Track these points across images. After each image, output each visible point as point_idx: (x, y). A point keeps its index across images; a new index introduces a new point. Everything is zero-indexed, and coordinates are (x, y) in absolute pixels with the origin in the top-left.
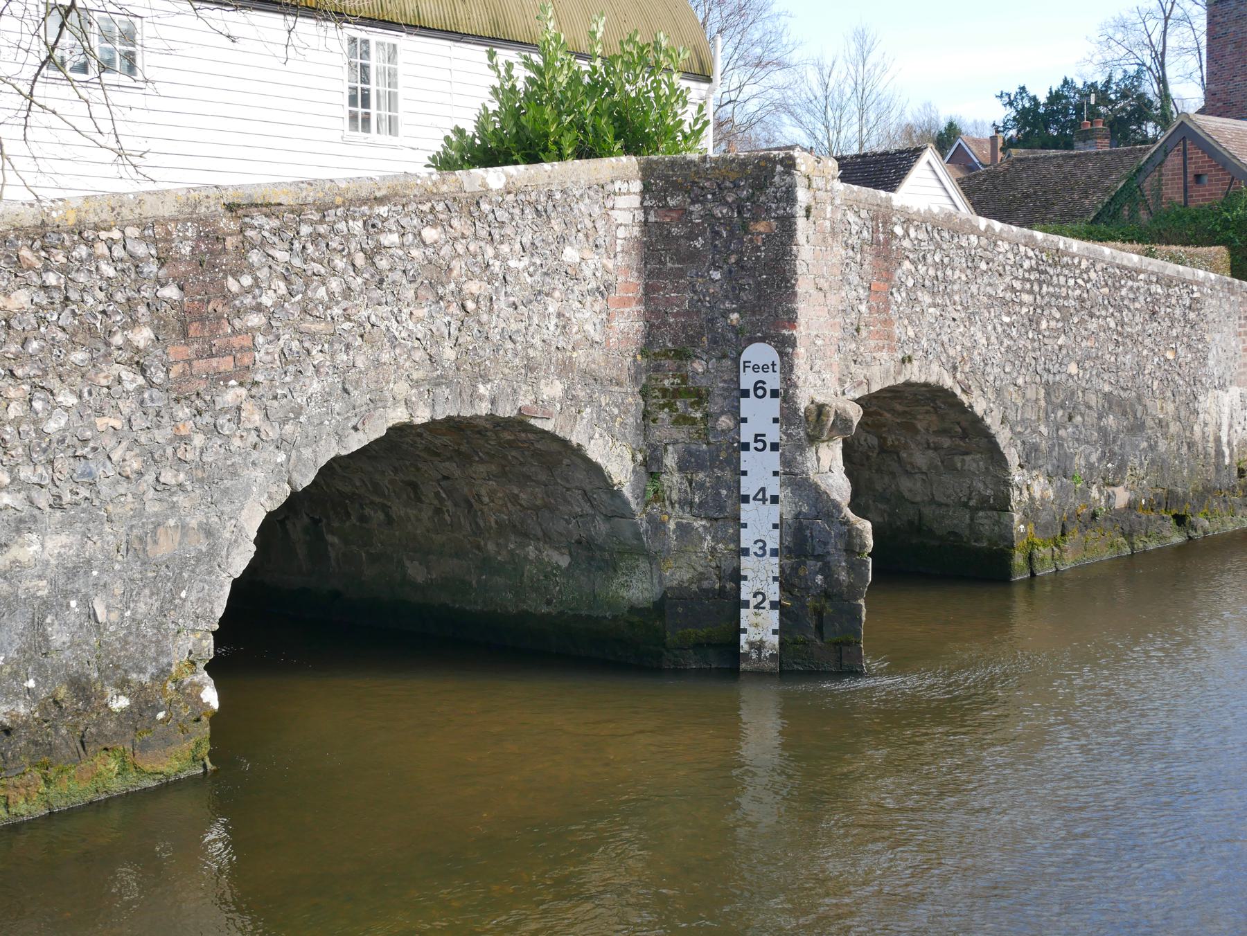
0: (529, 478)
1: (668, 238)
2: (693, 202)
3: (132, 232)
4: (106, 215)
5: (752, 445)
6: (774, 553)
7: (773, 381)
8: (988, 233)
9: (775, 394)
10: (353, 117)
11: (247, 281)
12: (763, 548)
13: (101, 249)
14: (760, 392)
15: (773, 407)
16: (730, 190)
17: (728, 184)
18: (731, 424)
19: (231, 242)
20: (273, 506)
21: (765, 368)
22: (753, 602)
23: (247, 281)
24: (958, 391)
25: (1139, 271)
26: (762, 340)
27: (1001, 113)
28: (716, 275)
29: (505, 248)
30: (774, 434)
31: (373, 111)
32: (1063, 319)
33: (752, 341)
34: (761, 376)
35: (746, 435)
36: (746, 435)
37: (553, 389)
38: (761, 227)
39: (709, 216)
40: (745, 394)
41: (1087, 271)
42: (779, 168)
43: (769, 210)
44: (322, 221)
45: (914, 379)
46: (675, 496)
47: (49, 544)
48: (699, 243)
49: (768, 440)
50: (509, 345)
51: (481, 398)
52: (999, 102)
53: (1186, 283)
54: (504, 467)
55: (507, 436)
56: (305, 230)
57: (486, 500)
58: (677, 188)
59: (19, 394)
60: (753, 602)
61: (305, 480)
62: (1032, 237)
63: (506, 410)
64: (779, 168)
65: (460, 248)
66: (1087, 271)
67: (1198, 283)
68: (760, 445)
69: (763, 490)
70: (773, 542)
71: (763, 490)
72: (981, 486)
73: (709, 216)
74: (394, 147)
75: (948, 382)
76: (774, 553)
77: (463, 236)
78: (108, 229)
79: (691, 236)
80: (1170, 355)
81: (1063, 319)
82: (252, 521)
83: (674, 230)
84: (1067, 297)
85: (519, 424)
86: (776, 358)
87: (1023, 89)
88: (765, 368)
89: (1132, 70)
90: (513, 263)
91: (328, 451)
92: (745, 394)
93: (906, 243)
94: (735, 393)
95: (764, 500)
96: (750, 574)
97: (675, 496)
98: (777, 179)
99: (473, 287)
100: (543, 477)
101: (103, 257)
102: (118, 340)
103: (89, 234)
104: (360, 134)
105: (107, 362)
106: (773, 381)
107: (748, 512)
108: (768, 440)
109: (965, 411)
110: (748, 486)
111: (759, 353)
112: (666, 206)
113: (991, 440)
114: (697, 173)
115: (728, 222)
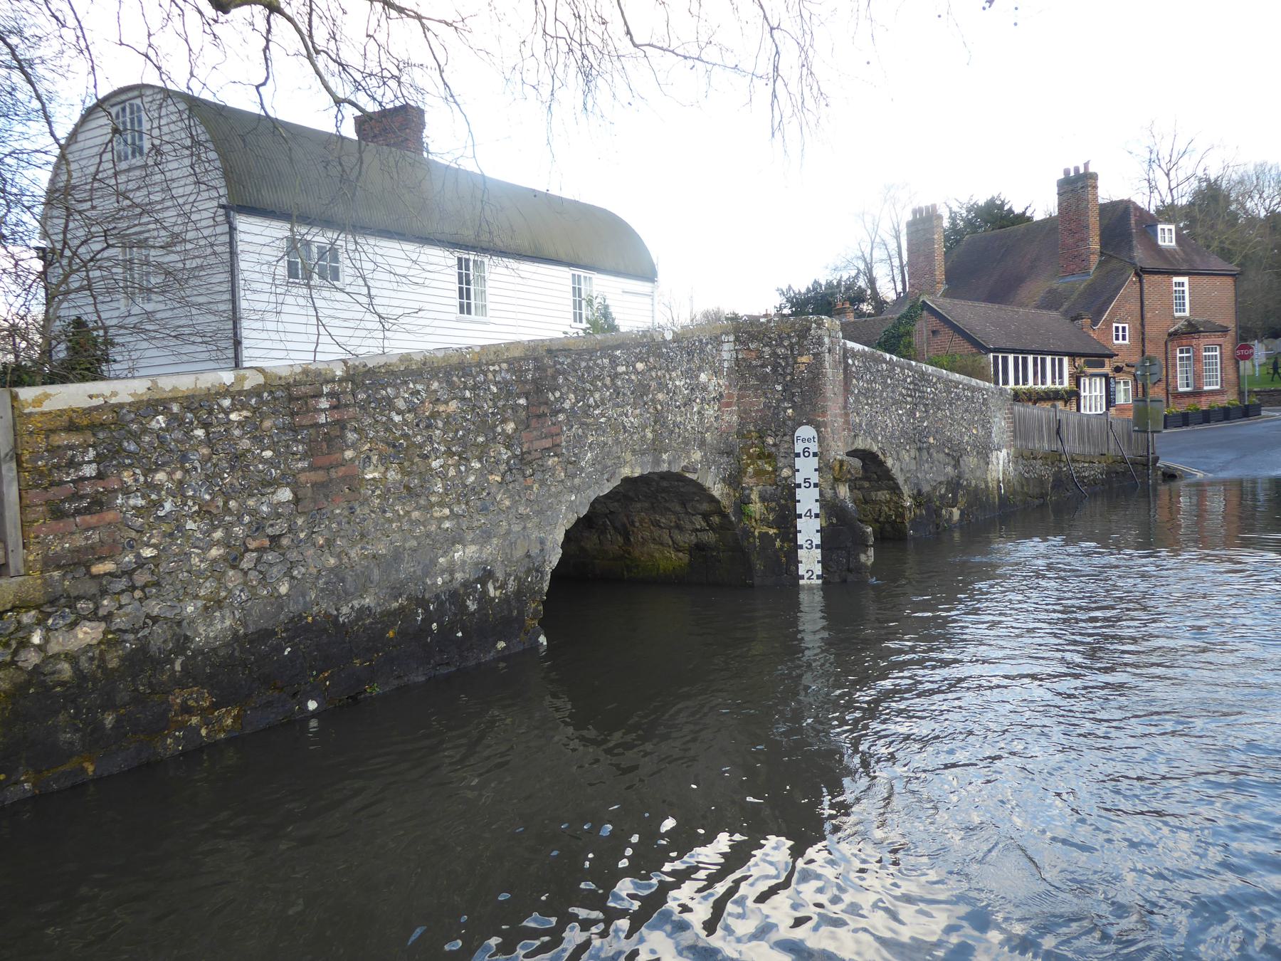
0: (669, 510)
1: (749, 366)
2: (764, 346)
3: (504, 366)
4: (492, 357)
5: (803, 485)
6: (817, 547)
7: (814, 447)
8: (890, 362)
9: (815, 455)
10: (461, 306)
11: (558, 394)
12: (811, 544)
13: (490, 376)
14: (807, 454)
15: (814, 462)
16: (786, 338)
17: (784, 335)
18: (790, 473)
19: (550, 371)
20: (568, 526)
21: (809, 440)
22: (806, 576)
23: (558, 394)
24: (880, 454)
25: (960, 383)
26: (807, 424)
27: (779, 300)
28: (779, 388)
29: (674, 374)
30: (815, 478)
31: (473, 301)
32: (926, 411)
33: (801, 424)
34: (807, 444)
35: (799, 479)
36: (799, 479)
37: (697, 455)
38: (804, 359)
39: (774, 354)
40: (798, 455)
41: (935, 383)
42: (814, 325)
43: (808, 350)
44: (590, 360)
45: (860, 447)
46: (758, 517)
47: (467, 551)
48: (768, 370)
49: (812, 482)
50: (677, 430)
51: (664, 461)
52: (777, 293)
53: (980, 389)
54: (652, 504)
55: (665, 484)
56: (583, 364)
57: (637, 524)
58: (753, 337)
59: (454, 462)
60: (806, 576)
61: (584, 511)
62: (911, 365)
63: (676, 469)
64: (814, 325)
65: (654, 374)
66: (935, 383)
67: (985, 390)
68: (807, 485)
69: (810, 510)
70: (817, 540)
71: (810, 510)
72: (887, 509)
73: (774, 354)
74: (485, 323)
75: (875, 449)
76: (817, 547)
77: (655, 367)
78: (493, 365)
79: (763, 366)
80: (975, 432)
81: (926, 411)
82: (560, 536)
83: (754, 363)
84: (927, 399)
85: (679, 477)
86: (815, 434)
87: (790, 287)
88: (809, 440)
89: (853, 273)
90: (677, 383)
91: (593, 494)
92: (798, 455)
93: (854, 369)
94: (792, 455)
95: (811, 516)
96: (804, 560)
97: (758, 517)
98: (812, 332)
99: (660, 396)
100: (678, 508)
101: (491, 381)
102: (499, 429)
103: (484, 368)
104: (465, 315)
105: (495, 443)
106: (814, 447)
107: (800, 524)
108: (812, 482)
109: (881, 464)
110: (800, 509)
111: (806, 432)
112: (749, 349)
113: (892, 479)
114: (766, 329)
115: (785, 358)
